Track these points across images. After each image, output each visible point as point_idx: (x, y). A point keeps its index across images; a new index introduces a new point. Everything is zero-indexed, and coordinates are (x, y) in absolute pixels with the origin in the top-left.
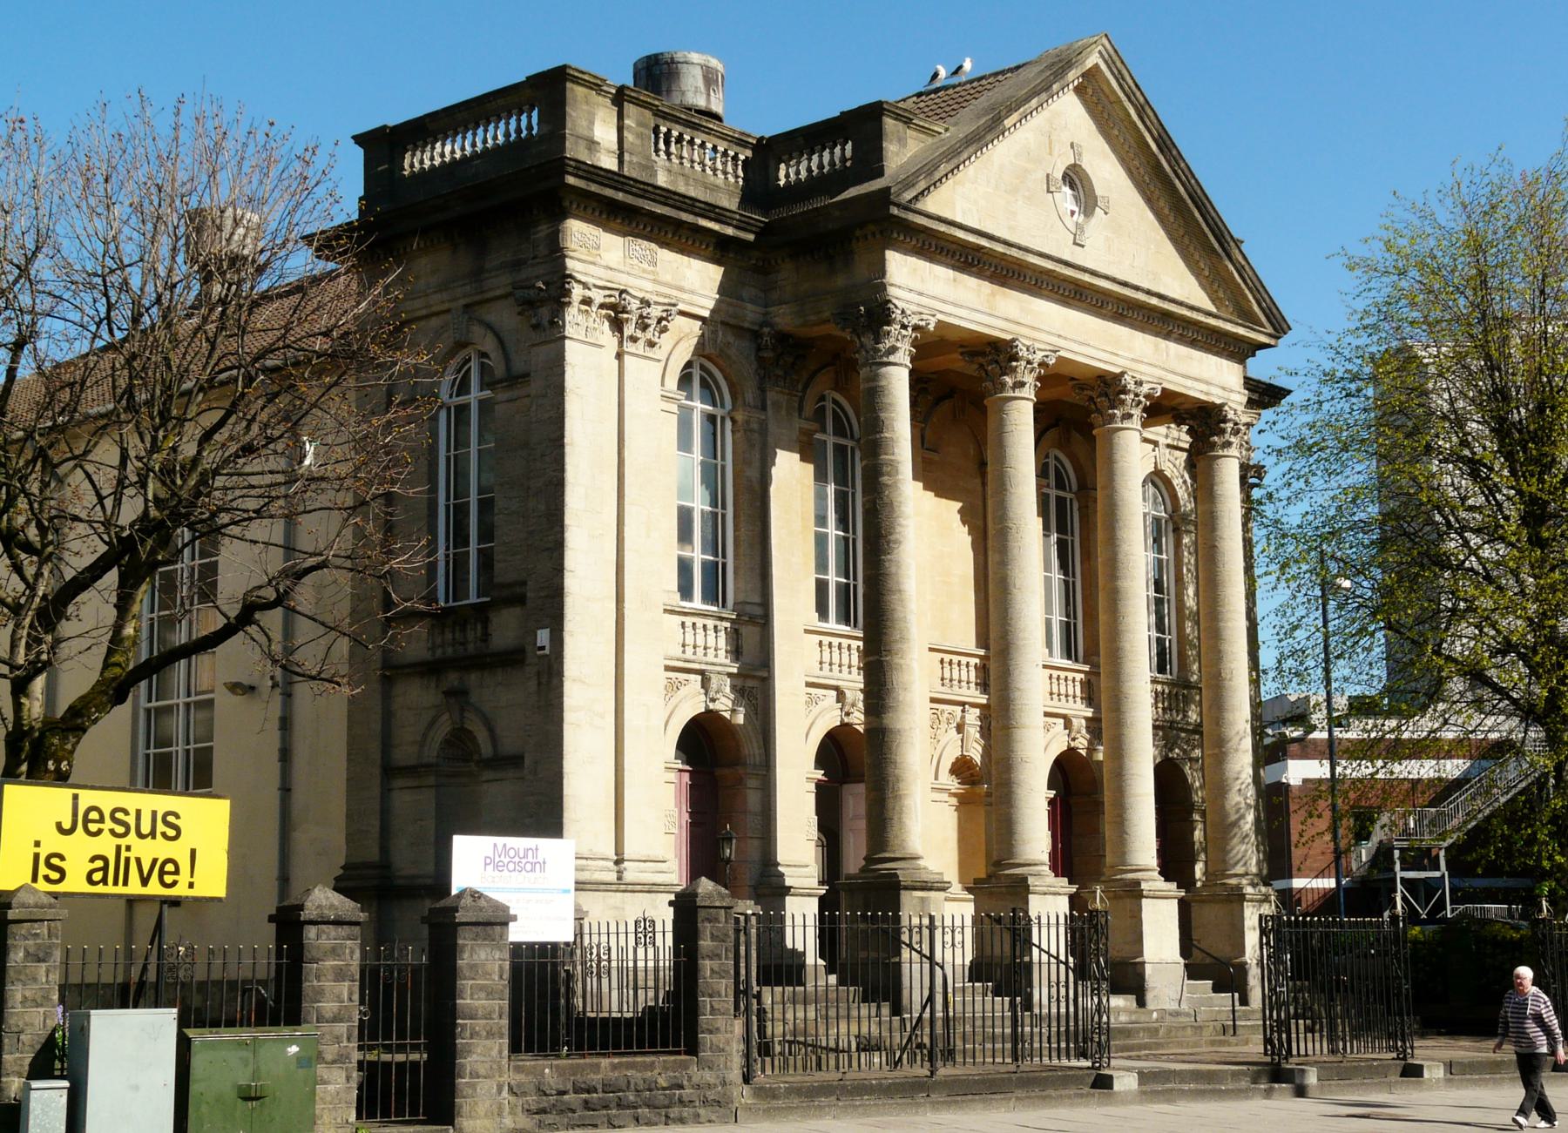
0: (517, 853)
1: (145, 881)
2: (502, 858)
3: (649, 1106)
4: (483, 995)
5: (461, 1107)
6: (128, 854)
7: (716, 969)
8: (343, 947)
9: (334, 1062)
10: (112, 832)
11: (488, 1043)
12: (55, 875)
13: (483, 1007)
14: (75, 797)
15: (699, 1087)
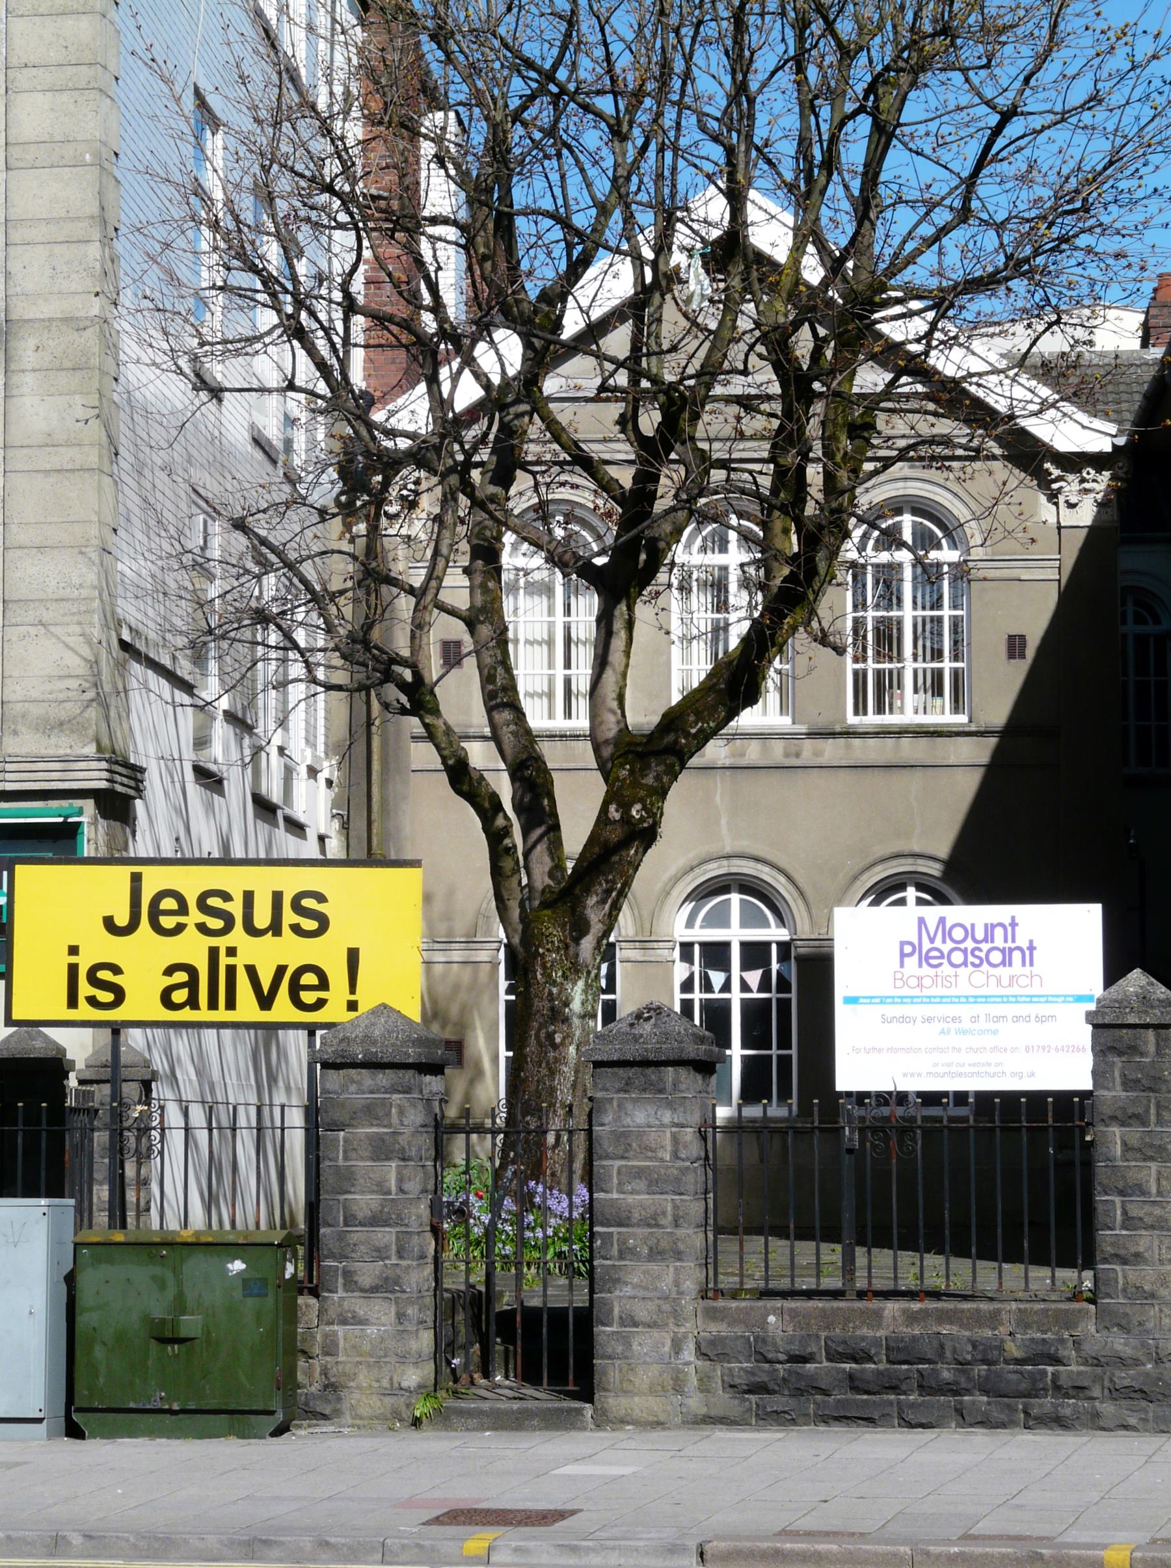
0: (969, 932)
1: (266, 1002)
2: (938, 943)
3: (986, 1392)
4: (641, 1185)
5: (605, 1373)
6: (231, 961)
7: (1134, 1141)
8: (386, 1104)
9: (374, 1289)
10: (202, 928)
11: (654, 1267)
12: (106, 997)
13: (641, 1205)
14: (136, 879)
15: (1097, 1362)
